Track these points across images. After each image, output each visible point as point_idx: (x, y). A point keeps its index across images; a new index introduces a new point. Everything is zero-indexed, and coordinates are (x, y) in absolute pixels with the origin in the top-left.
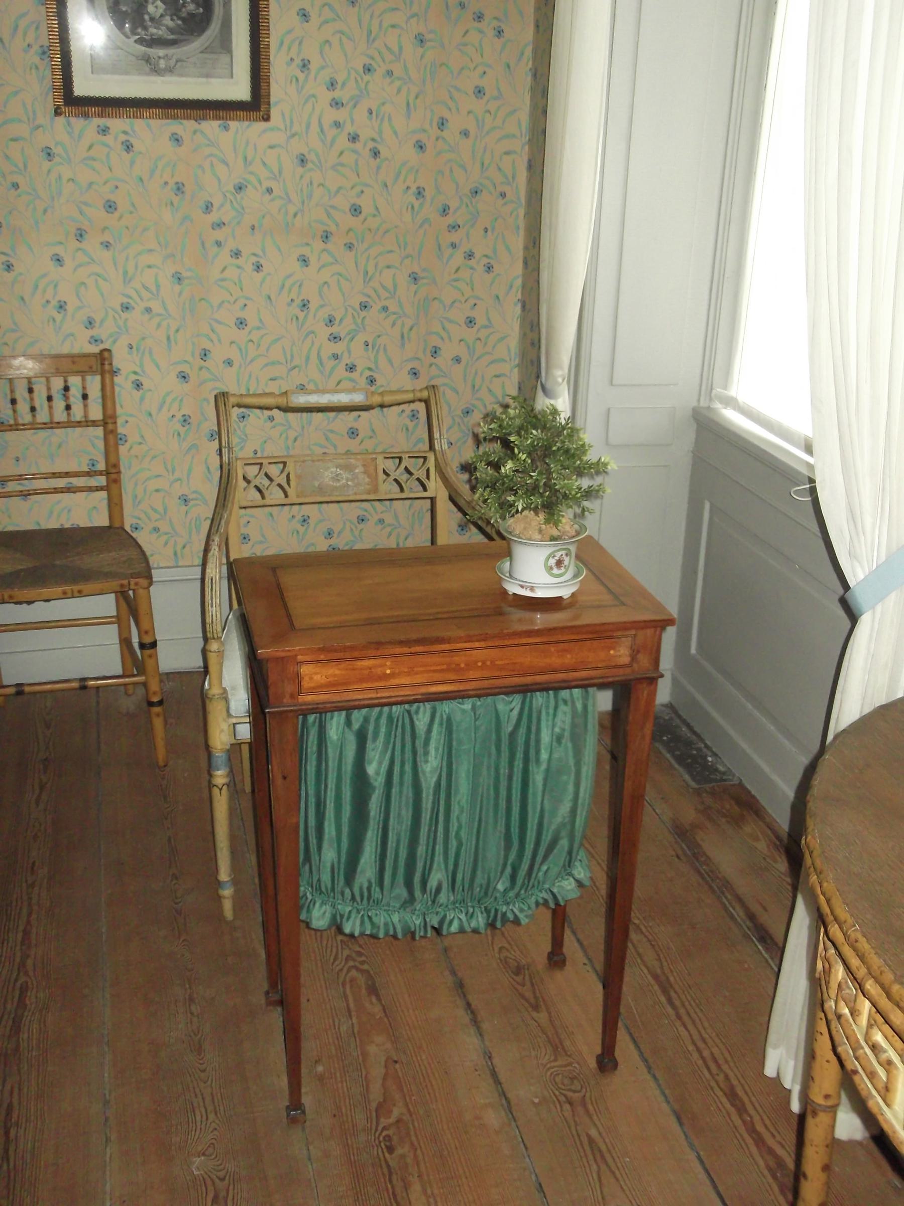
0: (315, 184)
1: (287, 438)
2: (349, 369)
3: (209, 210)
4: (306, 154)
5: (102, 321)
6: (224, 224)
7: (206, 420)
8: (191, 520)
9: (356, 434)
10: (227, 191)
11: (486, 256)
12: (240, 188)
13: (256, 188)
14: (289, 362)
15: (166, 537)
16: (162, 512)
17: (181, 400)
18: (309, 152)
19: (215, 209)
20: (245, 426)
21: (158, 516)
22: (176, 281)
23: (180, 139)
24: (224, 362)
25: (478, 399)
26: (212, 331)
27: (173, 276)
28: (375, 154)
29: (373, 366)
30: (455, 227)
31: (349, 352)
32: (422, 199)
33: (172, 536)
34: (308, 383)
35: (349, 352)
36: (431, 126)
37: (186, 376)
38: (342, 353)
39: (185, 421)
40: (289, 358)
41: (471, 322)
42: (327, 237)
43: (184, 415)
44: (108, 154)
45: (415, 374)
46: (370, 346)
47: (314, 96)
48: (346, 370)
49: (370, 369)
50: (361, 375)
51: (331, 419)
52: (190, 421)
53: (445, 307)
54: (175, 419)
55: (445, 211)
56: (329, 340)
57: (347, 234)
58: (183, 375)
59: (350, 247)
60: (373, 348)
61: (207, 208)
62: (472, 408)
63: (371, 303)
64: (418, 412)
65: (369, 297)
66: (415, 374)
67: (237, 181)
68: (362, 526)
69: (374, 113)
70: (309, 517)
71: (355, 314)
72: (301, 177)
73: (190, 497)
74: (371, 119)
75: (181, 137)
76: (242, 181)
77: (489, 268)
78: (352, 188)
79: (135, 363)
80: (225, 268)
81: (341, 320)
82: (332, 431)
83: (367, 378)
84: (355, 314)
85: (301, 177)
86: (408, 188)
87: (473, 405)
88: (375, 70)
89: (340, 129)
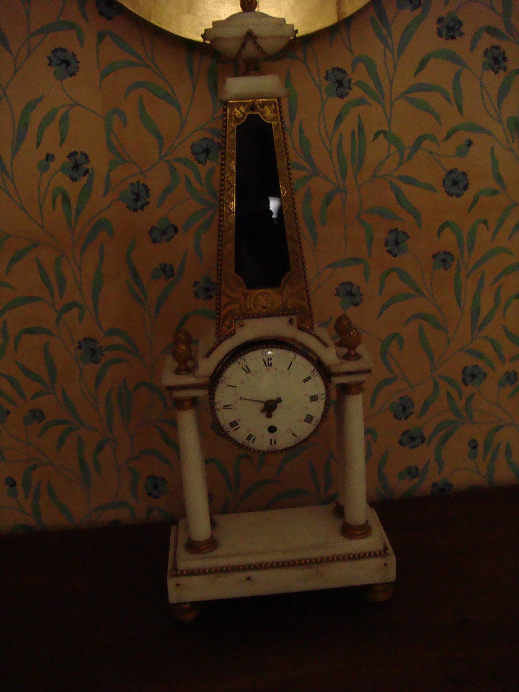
0: (370, 134)
2: (444, 32)
3: (140, 204)
4: (347, 68)
5: (426, 406)
6: (176, 229)
9: (461, 185)
17: (64, 119)
18: (354, 65)
27: (80, 347)
28: (496, 61)
29: (499, 23)
32: (84, 180)
34: (354, 65)
43: (72, 155)
44: (457, 76)
46: (480, 449)
48: (440, 34)
49: (492, 31)
50: (473, 46)
51: (407, 152)
56: (401, 442)
59: (444, 261)
60: (485, 453)
61: (137, 197)
65: (481, 356)
72: (339, 119)
75: (74, 55)
78: (448, 137)
81: (426, 406)
83: (485, 53)
85: (339, 119)
86: (49, 157)
88: (485, 375)
89: (419, 11)
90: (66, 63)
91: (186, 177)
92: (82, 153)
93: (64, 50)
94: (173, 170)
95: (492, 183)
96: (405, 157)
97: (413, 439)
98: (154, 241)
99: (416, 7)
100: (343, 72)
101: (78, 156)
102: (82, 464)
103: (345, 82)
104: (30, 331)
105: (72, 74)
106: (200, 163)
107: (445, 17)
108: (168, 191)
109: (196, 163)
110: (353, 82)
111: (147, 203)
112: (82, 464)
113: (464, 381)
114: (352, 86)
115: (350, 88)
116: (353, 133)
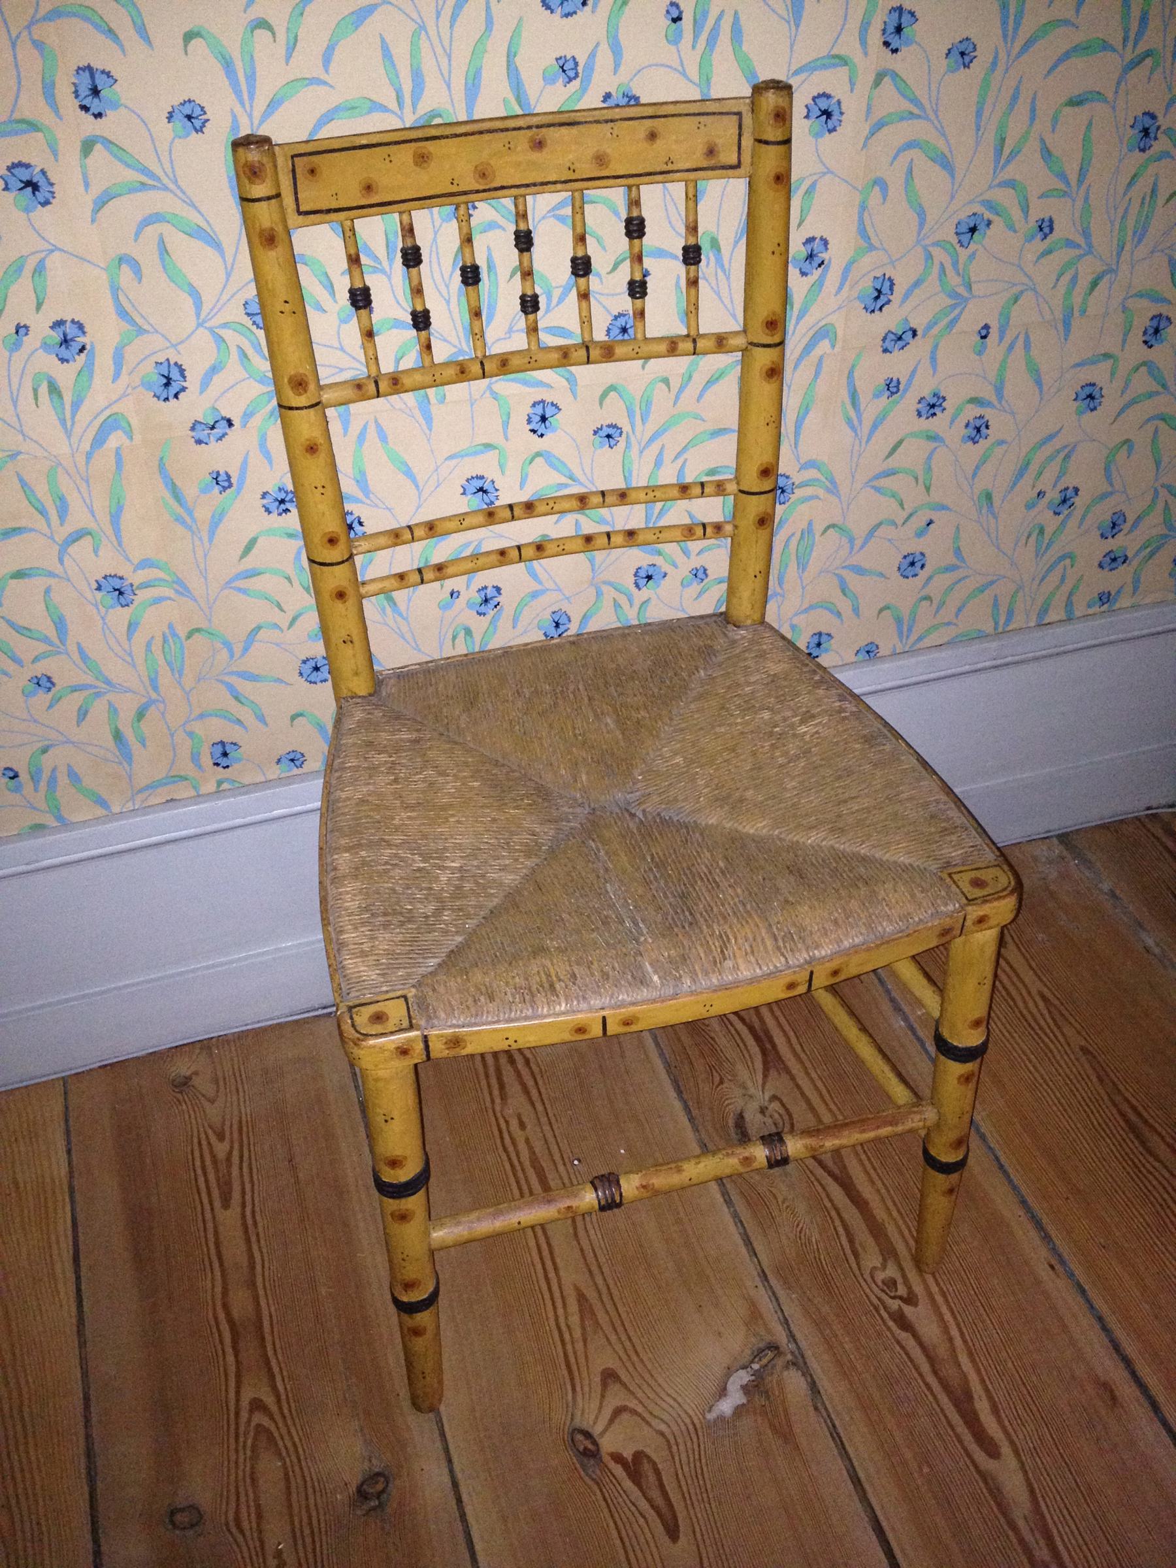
1: (1074, 280)
3: (173, 389)
7: (141, 331)
8: (148, 645)
10: (225, 325)
11: (974, 401)
12: (973, 230)
13: (1012, 228)
14: (408, 101)
15: (78, 698)
16: (52, 633)
17: (40, 269)
19: (193, 381)
20: (972, 256)
21: (42, 647)
22: (111, 599)
23: (42, 183)
24: (170, 117)
25: (1010, 184)
26: (237, 698)
27: (99, 588)
30: (899, 339)
31: (616, 50)
33: (98, 695)
35: (616, 50)
36: (863, 42)
37: (833, 108)
38: (592, 55)
39: (65, 341)
40: (1134, 26)
41: (912, 564)
42: (544, 419)
43: (59, 324)
45: (827, 114)
47: (1069, 556)
52: (824, 256)
53: (851, 540)
54: (30, 342)
55: (879, 297)
57: (601, 404)
58: (25, 175)
60: (697, 25)
62: (988, 215)
63: (666, 567)
64: (825, 242)
66: (827, 114)
67: (963, 215)
68: (646, 592)
69: (687, 18)
70: (498, 589)
71: (623, 600)
73: (137, 578)
74: (675, 40)
76: (978, 208)
77: (978, 430)
79: (684, 74)
82: (859, 570)
84: (623, 600)
87: (990, 205)
89: (576, 83)
90: (32, 185)
91: (942, 264)
92: (822, 239)
93: (828, 96)
94: (220, 339)
95: (951, 559)
97: (1114, 560)
99: (570, 80)
100: (1153, 117)
101: (68, 324)
102: (118, 736)
103: (1152, 130)
104: (19, 575)
105: (46, 203)
106: (962, 246)
107: (614, 94)
108: (214, 370)
109: (957, 246)
110: (1163, 128)
111: (184, 389)
112: (118, 736)
113: (637, 586)
114: (1159, 135)
115: (1156, 138)
116: (1144, 198)
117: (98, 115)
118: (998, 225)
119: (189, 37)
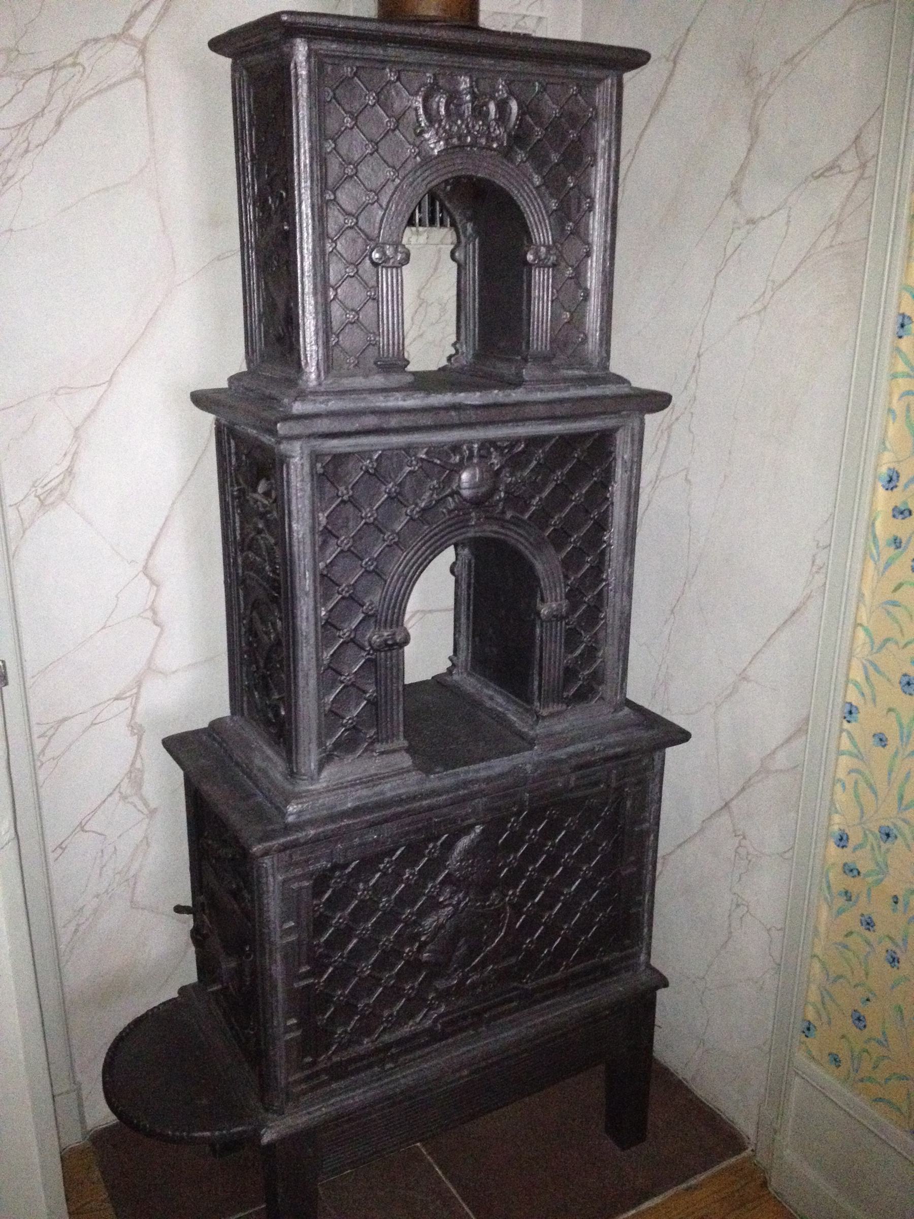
3: (891, 485)
80: (900, 586)
87: (898, 829)
96: (874, 651)
98: (894, 516)
117: (807, 1036)
118: (900, 840)
119: (890, 710)
